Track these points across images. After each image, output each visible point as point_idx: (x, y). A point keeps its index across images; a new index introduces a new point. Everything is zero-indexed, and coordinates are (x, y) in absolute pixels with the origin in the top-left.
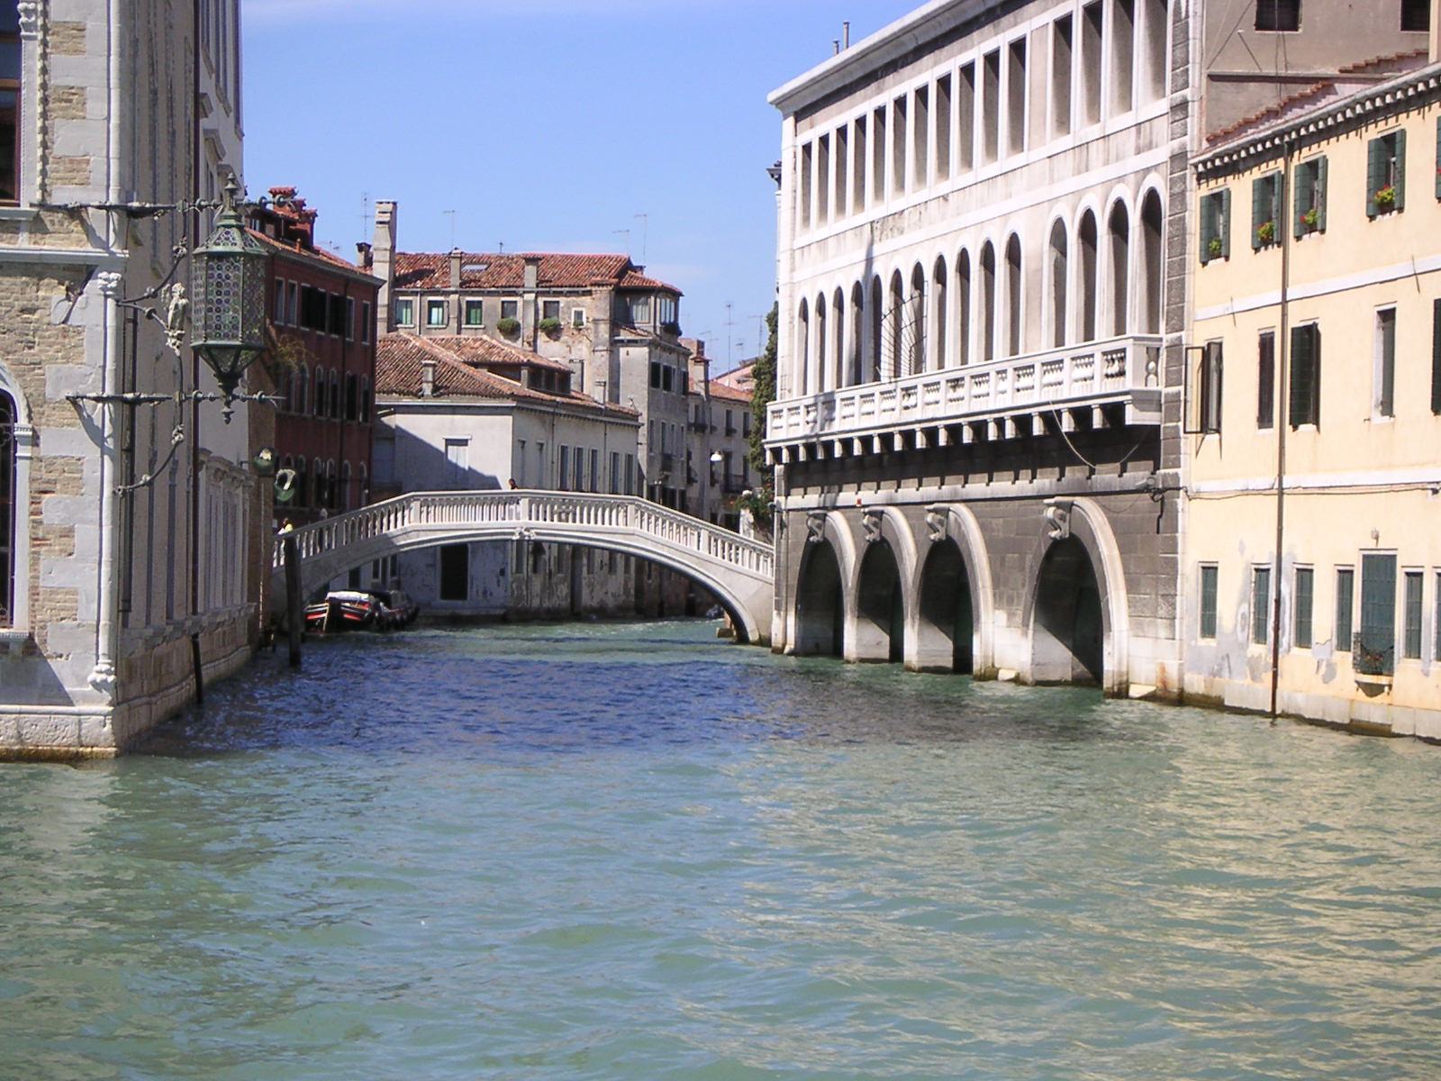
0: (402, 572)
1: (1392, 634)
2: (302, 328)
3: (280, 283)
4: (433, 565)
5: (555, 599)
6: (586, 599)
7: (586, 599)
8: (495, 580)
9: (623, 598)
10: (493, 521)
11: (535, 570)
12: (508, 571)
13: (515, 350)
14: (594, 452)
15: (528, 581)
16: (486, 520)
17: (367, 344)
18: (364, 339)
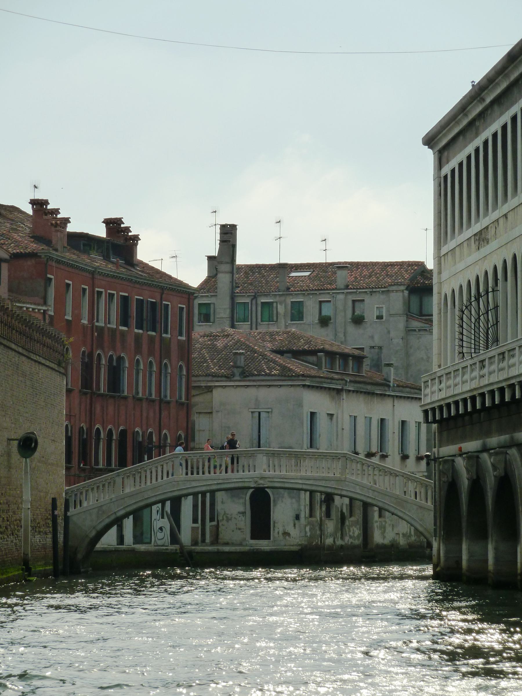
0: (220, 518)
1: (198, 515)
2: (121, 328)
3: (100, 293)
4: (244, 513)
5: (347, 539)
6: (378, 538)
7: (378, 538)
8: (292, 524)
9: (413, 538)
10: (247, 472)
11: (328, 515)
12: (302, 516)
13: (323, 338)
14: (382, 420)
15: (321, 524)
16: (241, 473)
17: (184, 338)
18: (181, 334)
